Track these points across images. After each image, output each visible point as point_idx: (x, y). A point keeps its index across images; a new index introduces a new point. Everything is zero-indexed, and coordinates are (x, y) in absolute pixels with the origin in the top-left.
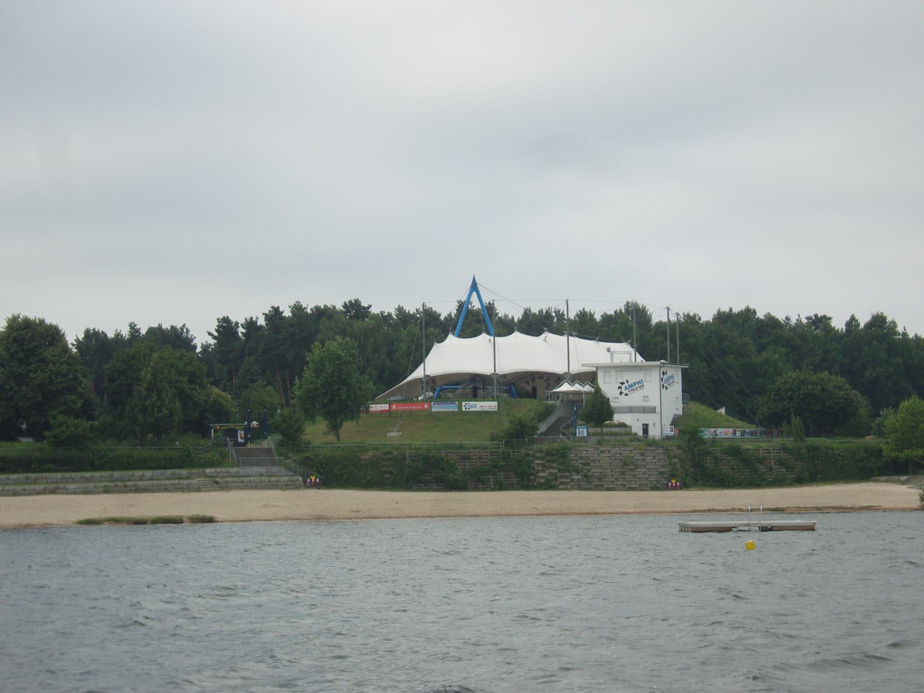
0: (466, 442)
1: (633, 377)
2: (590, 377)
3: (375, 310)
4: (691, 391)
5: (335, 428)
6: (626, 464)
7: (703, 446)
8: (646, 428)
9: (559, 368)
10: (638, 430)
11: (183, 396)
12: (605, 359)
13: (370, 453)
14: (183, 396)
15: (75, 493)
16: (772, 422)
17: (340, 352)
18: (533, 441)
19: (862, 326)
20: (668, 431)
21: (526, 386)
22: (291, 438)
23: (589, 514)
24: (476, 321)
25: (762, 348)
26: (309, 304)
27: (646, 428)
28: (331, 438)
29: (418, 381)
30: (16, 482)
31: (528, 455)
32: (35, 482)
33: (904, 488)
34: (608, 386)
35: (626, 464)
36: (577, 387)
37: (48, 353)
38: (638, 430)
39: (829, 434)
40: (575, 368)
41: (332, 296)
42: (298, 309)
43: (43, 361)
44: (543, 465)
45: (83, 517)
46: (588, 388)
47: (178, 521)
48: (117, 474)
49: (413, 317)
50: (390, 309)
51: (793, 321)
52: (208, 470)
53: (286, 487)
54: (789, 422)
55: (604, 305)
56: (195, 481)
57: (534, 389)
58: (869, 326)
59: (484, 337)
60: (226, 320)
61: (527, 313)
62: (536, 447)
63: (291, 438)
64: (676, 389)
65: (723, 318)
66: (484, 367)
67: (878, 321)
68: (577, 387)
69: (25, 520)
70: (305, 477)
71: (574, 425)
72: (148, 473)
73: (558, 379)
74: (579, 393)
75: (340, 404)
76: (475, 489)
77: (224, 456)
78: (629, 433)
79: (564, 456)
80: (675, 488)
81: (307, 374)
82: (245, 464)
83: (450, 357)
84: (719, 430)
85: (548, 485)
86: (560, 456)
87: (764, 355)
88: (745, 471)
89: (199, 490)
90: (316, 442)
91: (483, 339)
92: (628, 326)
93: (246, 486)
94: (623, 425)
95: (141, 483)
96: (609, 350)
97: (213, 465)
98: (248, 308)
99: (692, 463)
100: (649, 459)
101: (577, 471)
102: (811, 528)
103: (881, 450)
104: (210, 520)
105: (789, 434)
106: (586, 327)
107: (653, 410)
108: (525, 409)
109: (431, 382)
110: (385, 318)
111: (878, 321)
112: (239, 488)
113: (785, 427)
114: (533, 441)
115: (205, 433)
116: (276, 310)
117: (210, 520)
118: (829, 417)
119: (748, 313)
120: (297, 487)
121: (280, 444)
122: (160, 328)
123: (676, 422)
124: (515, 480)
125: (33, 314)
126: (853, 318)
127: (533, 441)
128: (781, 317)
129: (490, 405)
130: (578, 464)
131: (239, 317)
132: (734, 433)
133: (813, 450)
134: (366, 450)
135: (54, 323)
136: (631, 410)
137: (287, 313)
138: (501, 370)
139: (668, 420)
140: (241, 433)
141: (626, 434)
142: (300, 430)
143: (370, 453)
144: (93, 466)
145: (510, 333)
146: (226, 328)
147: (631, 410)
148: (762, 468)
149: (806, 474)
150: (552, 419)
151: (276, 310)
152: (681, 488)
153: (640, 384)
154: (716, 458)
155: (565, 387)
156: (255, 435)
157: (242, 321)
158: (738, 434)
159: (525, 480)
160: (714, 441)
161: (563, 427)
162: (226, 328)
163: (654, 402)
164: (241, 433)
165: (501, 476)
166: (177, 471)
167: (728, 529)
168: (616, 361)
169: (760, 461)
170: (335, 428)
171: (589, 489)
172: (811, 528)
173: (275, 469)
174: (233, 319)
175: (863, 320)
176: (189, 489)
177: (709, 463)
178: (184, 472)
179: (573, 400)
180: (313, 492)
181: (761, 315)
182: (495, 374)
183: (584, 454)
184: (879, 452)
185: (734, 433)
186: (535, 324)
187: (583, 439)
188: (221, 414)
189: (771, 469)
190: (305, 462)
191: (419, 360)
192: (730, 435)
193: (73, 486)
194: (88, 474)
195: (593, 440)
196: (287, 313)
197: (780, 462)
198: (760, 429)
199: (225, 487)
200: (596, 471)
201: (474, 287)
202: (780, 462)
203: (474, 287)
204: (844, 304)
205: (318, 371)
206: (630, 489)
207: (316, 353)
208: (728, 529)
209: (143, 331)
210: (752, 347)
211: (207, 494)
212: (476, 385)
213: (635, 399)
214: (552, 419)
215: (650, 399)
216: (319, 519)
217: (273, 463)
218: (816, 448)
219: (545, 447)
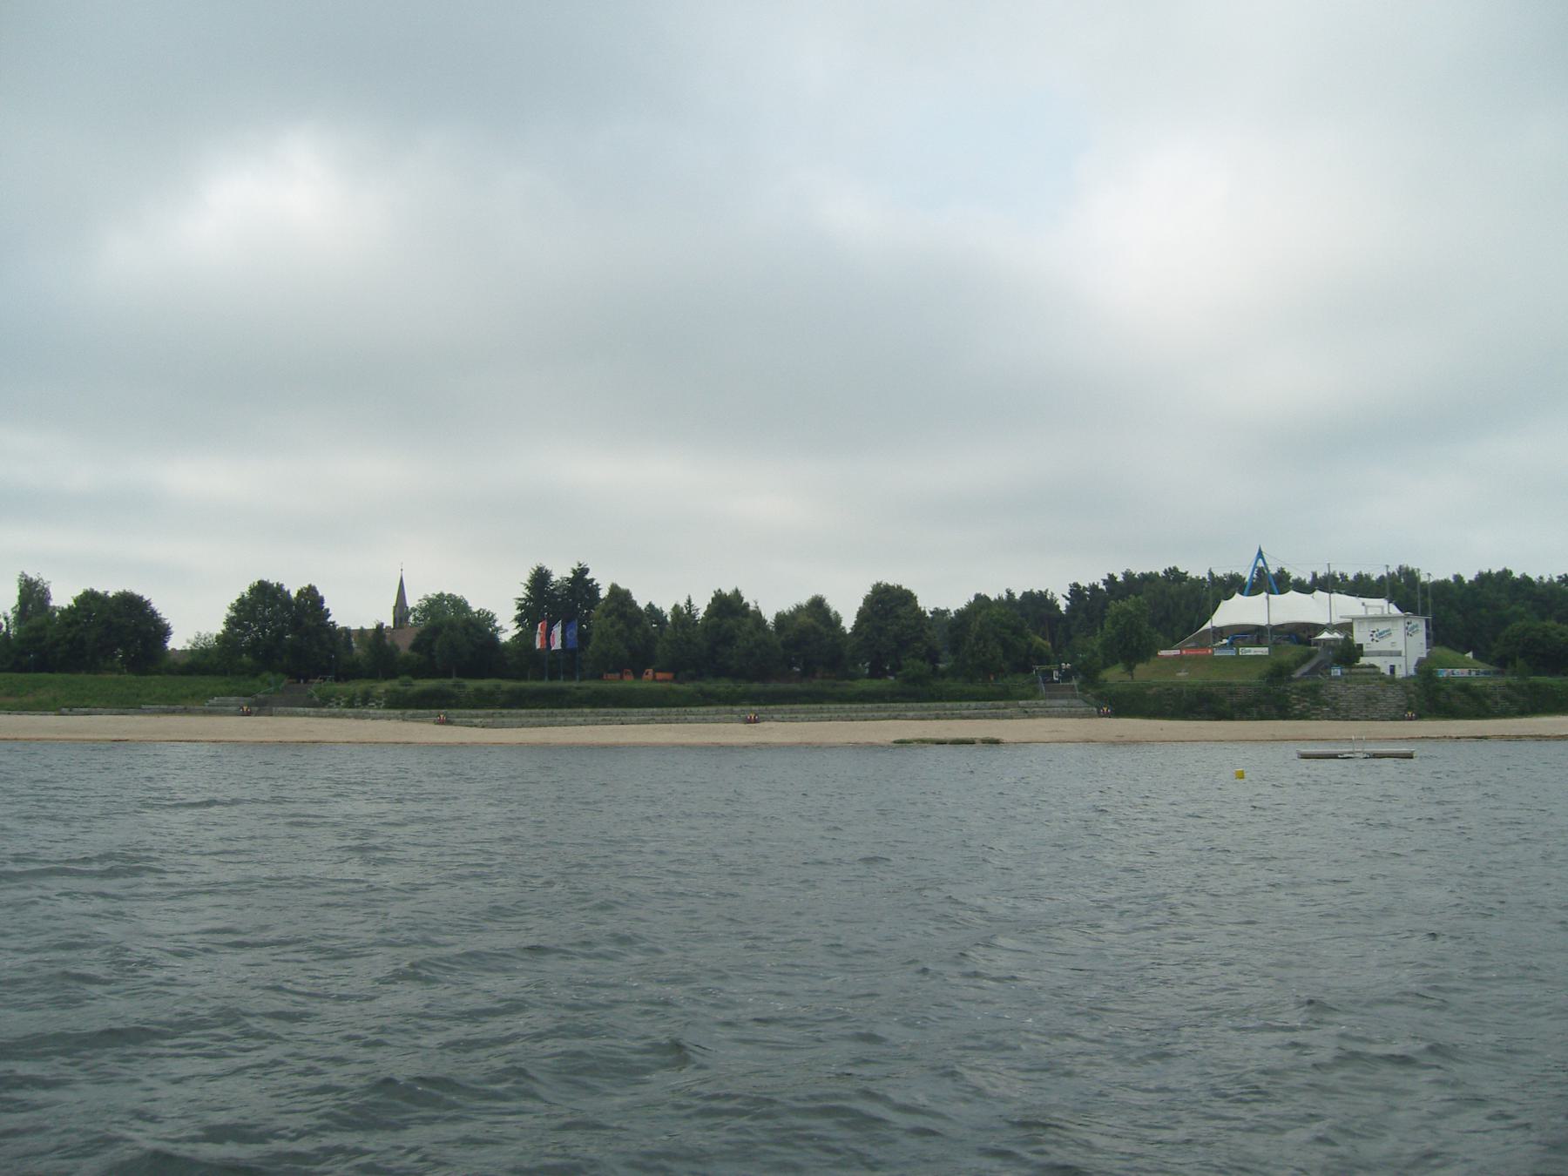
0: (1236, 680)
1: (1382, 627)
2: (1346, 628)
4: (1437, 636)
5: (1130, 669)
8: (1392, 669)
9: (1323, 620)
10: (1385, 670)
12: (1360, 612)
16: (1503, 663)
18: (1297, 679)
21: (1302, 633)
24: (1273, 582)
26: (1138, 570)
27: (1392, 669)
28: (1127, 677)
30: (871, 710)
32: (885, 710)
34: (1360, 636)
35: (1370, 699)
36: (1336, 635)
37: (901, 611)
40: (1336, 620)
41: (1157, 566)
43: (897, 617)
47: (971, 742)
48: (948, 705)
50: (1202, 573)
51: (1546, 580)
53: (1083, 716)
59: (1264, 594)
60: (1076, 585)
62: (1293, 684)
63: (1089, 674)
64: (1420, 637)
65: (1484, 579)
66: (1261, 620)
68: (1336, 635)
69: (817, 740)
72: (973, 704)
73: (1319, 628)
74: (1335, 640)
77: (1036, 691)
78: (1378, 673)
79: (1316, 692)
82: (1051, 698)
83: (1235, 611)
85: (1302, 716)
86: (1313, 692)
87: (1514, 608)
88: (1471, 703)
90: (1111, 681)
94: (1373, 666)
95: (965, 712)
97: (1027, 698)
99: (1429, 697)
104: (997, 742)
105: (1513, 674)
106: (1361, 587)
107: (1399, 654)
108: (1291, 652)
109: (1219, 632)
110: (1199, 582)
114: (1291, 680)
119: (1506, 574)
122: (1031, 592)
123: (1420, 662)
124: (1274, 711)
127: (1297, 679)
130: (1328, 698)
131: (1084, 583)
134: (1149, 687)
136: (1379, 654)
137: (1120, 579)
138: (1274, 622)
139: (1412, 662)
146: (1076, 591)
147: (1379, 654)
148: (1489, 702)
150: (1314, 662)
151: (1112, 577)
153: (1388, 633)
155: (1325, 635)
156: (1066, 676)
159: (1282, 711)
160: (1447, 680)
161: (1323, 668)
162: (1076, 591)
163: (1400, 647)
164: (1056, 673)
165: (1263, 708)
167: (1335, 756)
168: (1371, 613)
169: (1487, 696)
170: (1130, 669)
172: (1409, 756)
173: (1075, 702)
176: (1004, 717)
178: (1002, 703)
181: (1517, 575)
187: (1336, 678)
188: (1042, 658)
190: (1099, 697)
194: (925, 705)
196: (1120, 579)
197: (1505, 697)
198: (1493, 668)
199: (1032, 716)
201: (1260, 555)
202: (1505, 697)
203: (1260, 555)
208: (1335, 756)
209: (1018, 596)
212: (1255, 634)
213: (1384, 645)
214: (1314, 662)
215: (1397, 644)
219: (1299, 685)
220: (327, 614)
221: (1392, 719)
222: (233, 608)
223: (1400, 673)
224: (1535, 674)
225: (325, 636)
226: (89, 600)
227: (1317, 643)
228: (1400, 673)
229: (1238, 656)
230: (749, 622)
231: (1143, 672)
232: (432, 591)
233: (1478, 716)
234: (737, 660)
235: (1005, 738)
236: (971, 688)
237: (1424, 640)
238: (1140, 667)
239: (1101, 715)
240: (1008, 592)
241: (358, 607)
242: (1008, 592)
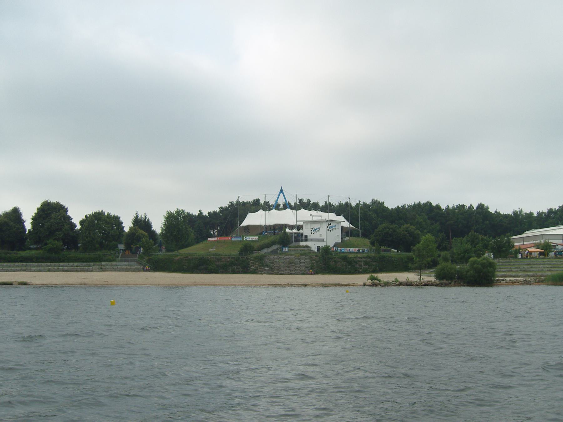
1: (316, 226)
6: (291, 263)
7: (330, 256)
13: (179, 257)
15: (34, 271)
19: (475, 208)
23: (333, 285)
30: (17, 266)
31: (248, 259)
34: (306, 231)
44: (253, 263)
45: (20, 281)
58: (477, 208)
67: (481, 206)
76: (222, 273)
80: (311, 274)
84: (351, 249)
85: (254, 272)
91: (261, 212)
93: (120, 270)
94: (307, 247)
96: (311, 215)
100: (302, 261)
101: (267, 266)
103: (413, 258)
104: (25, 284)
107: (323, 240)
111: (481, 206)
112: (111, 271)
119: (429, 204)
124: (241, 270)
125: (53, 200)
129: (256, 238)
132: (359, 250)
141: (308, 250)
143: (179, 257)
144: (69, 260)
145: (271, 210)
148: (357, 266)
149: (378, 268)
152: (314, 274)
154: (335, 261)
158: (361, 251)
159: (246, 270)
163: (324, 237)
166: (89, 263)
168: (315, 219)
169: (356, 262)
171: (273, 274)
173: (132, 263)
182: (265, 225)
183: (272, 258)
185: (359, 250)
189: (361, 266)
190: (149, 261)
192: (357, 251)
193: (34, 268)
197: (366, 263)
200: (276, 266)
202: (366, 263)
206: (291, 274)
211: (260, 275)
213: (316, 236)
216: (305, 285)
218: (384, 257)
220: (438, 207)
222: (214, 211)
230: (67, 227)
232: (90, 210)
233: (350, 273)
234: (98, 242)
239: (144, 270)
240: (200, 211)
242: (200, 211)
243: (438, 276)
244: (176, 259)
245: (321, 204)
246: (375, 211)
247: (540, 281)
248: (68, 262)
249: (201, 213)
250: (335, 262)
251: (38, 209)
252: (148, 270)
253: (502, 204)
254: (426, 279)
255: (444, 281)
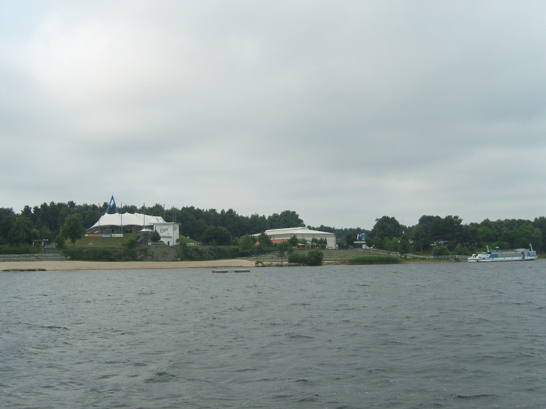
1: (165, 227)
2: (151, 227)
3: (77, 205)
4: (183, 231)
5: (73, 242)
8: (169, 243)
9: (141, 224)
10: (166, 243)
11: (26, 230)
12: (156, 222)
14: (26, 230)
16: (207, 241)
17: (77, 218)
18: (134, 246)
20: (175, 244)
21: (128, 229)
22: (60, 245)
24: (113, 210)
25: (197, 219)
26: (56, 202)
27: (169, 243)
28: (73, 245)
29: (97, 227)
33: (246, 261)
36: (147, 230)
38: (166, 243)
39: (222, 245)
42: (52, 204)
46: (150, 230)
47: (34, 270)
48: (6, 255)
49: (89, 207)
51: (205, 210)
52: (35, 255)
53: (60, 260)
54: (212, 241)
55: (150, 205)
56: (32, 258)
57: (131, 230)
60: (27, 206)
61: (143, 207)
62: (137, 248)
64: (177, 231)
67: (231, 211)
68: (147, 230)
70: (66, 257)
71: (147, 242)
72: (17, 255)
73: (140, 227)
75: (75, 233)
76: (119, 261)
78: (164, 244)
81: (65, 225)
83: (106, 220)
85: (141, 260)
86: (145, 251)
88: (198, 256)
89: (33, 261)
92: (156, 211)
93: (48, 260)
94: (162, 242)
97: (36, 253)
98: (35, 202)
99: (184, 254)
101: (150, 255)
102: (249, 271)
104: (44, 270)
105: (212, 245)
106: (145, 211)
107: (171, 237)
111: (231, 211)
113: (211, 243)
115: (30, 243)
116: (45, 204)
117: (44, 270)
118: (223, 240)
119: (192, 208)
120: (63, 260)
121: (57, 247)
123: (177, 241)
126: (223, 210)
127: (134, 246)
128: (202, 209)
129: (121, 235)
131: (32, 206)
133: (219, 249)
134: (84, 249)
135: (284, 210)
136: (164, 237)
137: (49, 205)
138: (123, 225)
140: (43, 243)
142: (64, 242)
146: (27, 209)
147: (164, 237)
148: (204, 255)
153: (167, 229)
157: (33, 207)
159: (134, 258)
160: (190, 247)
163: (171, 235)
164: (43, 243)
165: (127, 257)
167: (226, 272)
168: (159, 222)
170: (73, 242)
172: (249, 271)
173: (56, 254)
174: (30, 207)
175: (226, 210)
177: (189, 253)
178: (28, 255)
179: (146, 234)
180: (69, 261)
184: (238, 250)
186: (132, 210)
188: (35, 237)
191: (97, 220)
195: (154, 246)
196: (49, 205)
197: (210, 253)
198: (202, 243)
199: (41, 260)
200: (155, 256)
201: (112, 198)
203: (112, 198)
204: (220, 206)
205: (69, 223)
207: (69, 218)
208: (226, 272)
210: (194, 219)
212: (113, 229)
215: (170, 234)
217: (56, 253)
221: (173, 261)
223: (171, 244)
224: (219, 245)
225: (505, 230)
226: (183, 208)
227: (140, 233)
228: (171, 244)
229: (111, 237)
231: (78, 244)
235: (47, 269)
236: (12, 249)
237: (178, 232)
238: (77, 241)
241: (409, 220)
243: (290, 261)
244: (84, 251)
245: (139, 207)
246: (385, 221)
247: (344, 262)
248: (4, 254)
249: (27, 209)
250: (191, 252)
251: (298, 215)
252: (69, 260)
253: (244, 211)
254: (285, 263)
255: (293, 263)
